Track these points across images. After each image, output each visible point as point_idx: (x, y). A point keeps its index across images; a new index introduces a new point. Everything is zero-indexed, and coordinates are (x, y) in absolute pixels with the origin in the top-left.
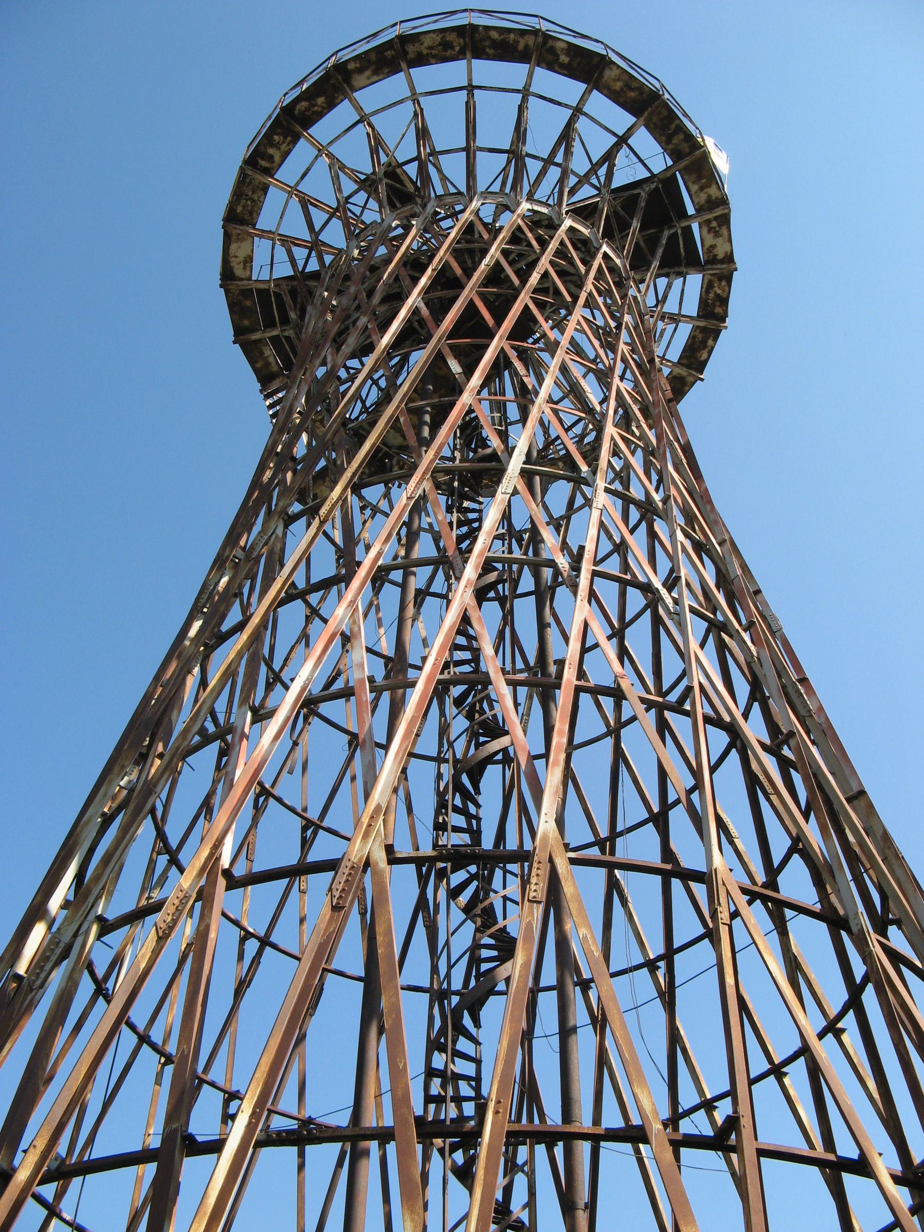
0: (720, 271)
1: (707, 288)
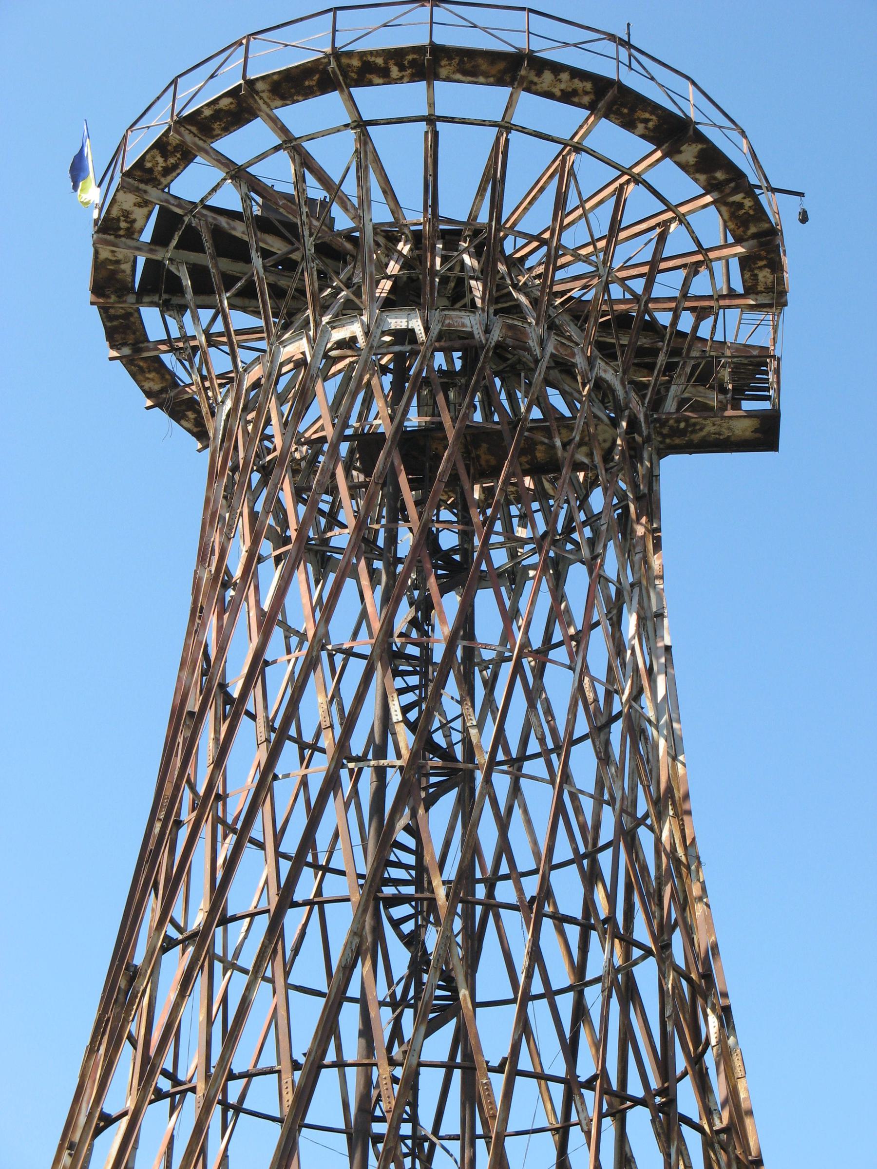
1: (171, 171)
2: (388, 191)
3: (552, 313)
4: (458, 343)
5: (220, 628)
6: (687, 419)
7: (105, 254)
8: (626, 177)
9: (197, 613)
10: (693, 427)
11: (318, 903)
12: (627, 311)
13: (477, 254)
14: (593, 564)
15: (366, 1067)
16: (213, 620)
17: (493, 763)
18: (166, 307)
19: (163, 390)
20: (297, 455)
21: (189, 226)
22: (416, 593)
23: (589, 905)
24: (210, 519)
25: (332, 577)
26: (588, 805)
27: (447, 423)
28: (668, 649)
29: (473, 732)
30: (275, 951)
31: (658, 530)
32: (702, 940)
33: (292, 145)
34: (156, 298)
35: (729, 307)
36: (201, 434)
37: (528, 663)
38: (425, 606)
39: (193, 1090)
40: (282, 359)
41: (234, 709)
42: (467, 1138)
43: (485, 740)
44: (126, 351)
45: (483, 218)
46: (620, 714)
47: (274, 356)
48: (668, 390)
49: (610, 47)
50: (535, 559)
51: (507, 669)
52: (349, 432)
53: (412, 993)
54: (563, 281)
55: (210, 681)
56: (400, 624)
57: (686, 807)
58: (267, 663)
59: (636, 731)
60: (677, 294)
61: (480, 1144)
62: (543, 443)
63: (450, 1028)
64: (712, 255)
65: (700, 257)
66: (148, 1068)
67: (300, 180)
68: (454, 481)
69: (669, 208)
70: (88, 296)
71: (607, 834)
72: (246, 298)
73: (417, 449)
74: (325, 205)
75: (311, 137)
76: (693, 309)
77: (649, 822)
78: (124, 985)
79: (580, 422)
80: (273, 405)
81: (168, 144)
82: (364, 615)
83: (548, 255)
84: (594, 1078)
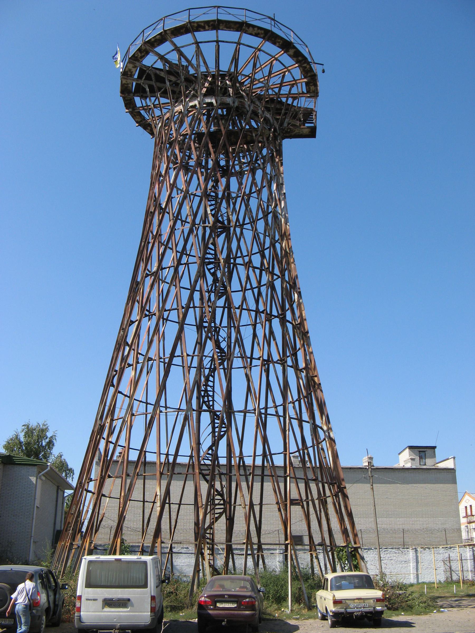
0: (135, 59)
1: (143, 57)
2: (205, 62)
3: (252, 98)
4: (225, 106)
5: (159, 188)
6: (290, 129)
7: (124, 82)
8: (273, 59)
9: (152, 184)
10: (292, 131)
11: (187, 264)
12: (273, 97)
13: (231, 81)
14: (264, 169)
15: (201, 308)
16: (157, 186)
17: (236, 226)
18: (142, 97)
19: (141, 121)
20: (179, 139)
21: (148, 73)
22: (213, 178)
23: (262, 264)
24: (155, 157)
25: (190, 174)
26: (262, 236)
27: (223, 129)
28: (285, 193)
29: (230, 216)
30: (176, 277)
31: (282, 160)
32: (293, 274)
33: (177, 49)
34: (139, 95)
35: (302, 97)
36: (152, 133)
37: (246, 197)
38: (217, 181)
39: (155, 314)
40: (175, 111)
41: (163, 211)
42: (229, 327)
43: (234, 218)
44: (131, 110)
45: (232, 70)
46: (271, 212)
47: (173, 110)
48: (285, 120)
49: (269, 21)
50: (248, 168)
51: (239, 200)
52: (194, 132)
53: (214, 288)
54: (255, 89)
55: (156, 203)
56: (209, 187)
57: (289, 237)
58: (172, 198)
59: (275, 217)
60: (287, 93)
61: (233, 328)
62: (249, 135)
63: (224, 298)
64: (297, 82)
65: (294, 82)
66: (143, 309)
67: (180, 59)
68: (224, 145)
69: (286, 68)
70: (119, 94)
71: (267, 245)
72: (164, 94)
73: (214, 137)
74: (187, 67)
75: (183, 47)
76: (292, 97)
77: (279, 241)
78: (135, 287)
79: (260, 129)
80: (173, 124)
81: (142, 49)
82: (199, 184)
83: (251, 81)
84: (264, 310)
